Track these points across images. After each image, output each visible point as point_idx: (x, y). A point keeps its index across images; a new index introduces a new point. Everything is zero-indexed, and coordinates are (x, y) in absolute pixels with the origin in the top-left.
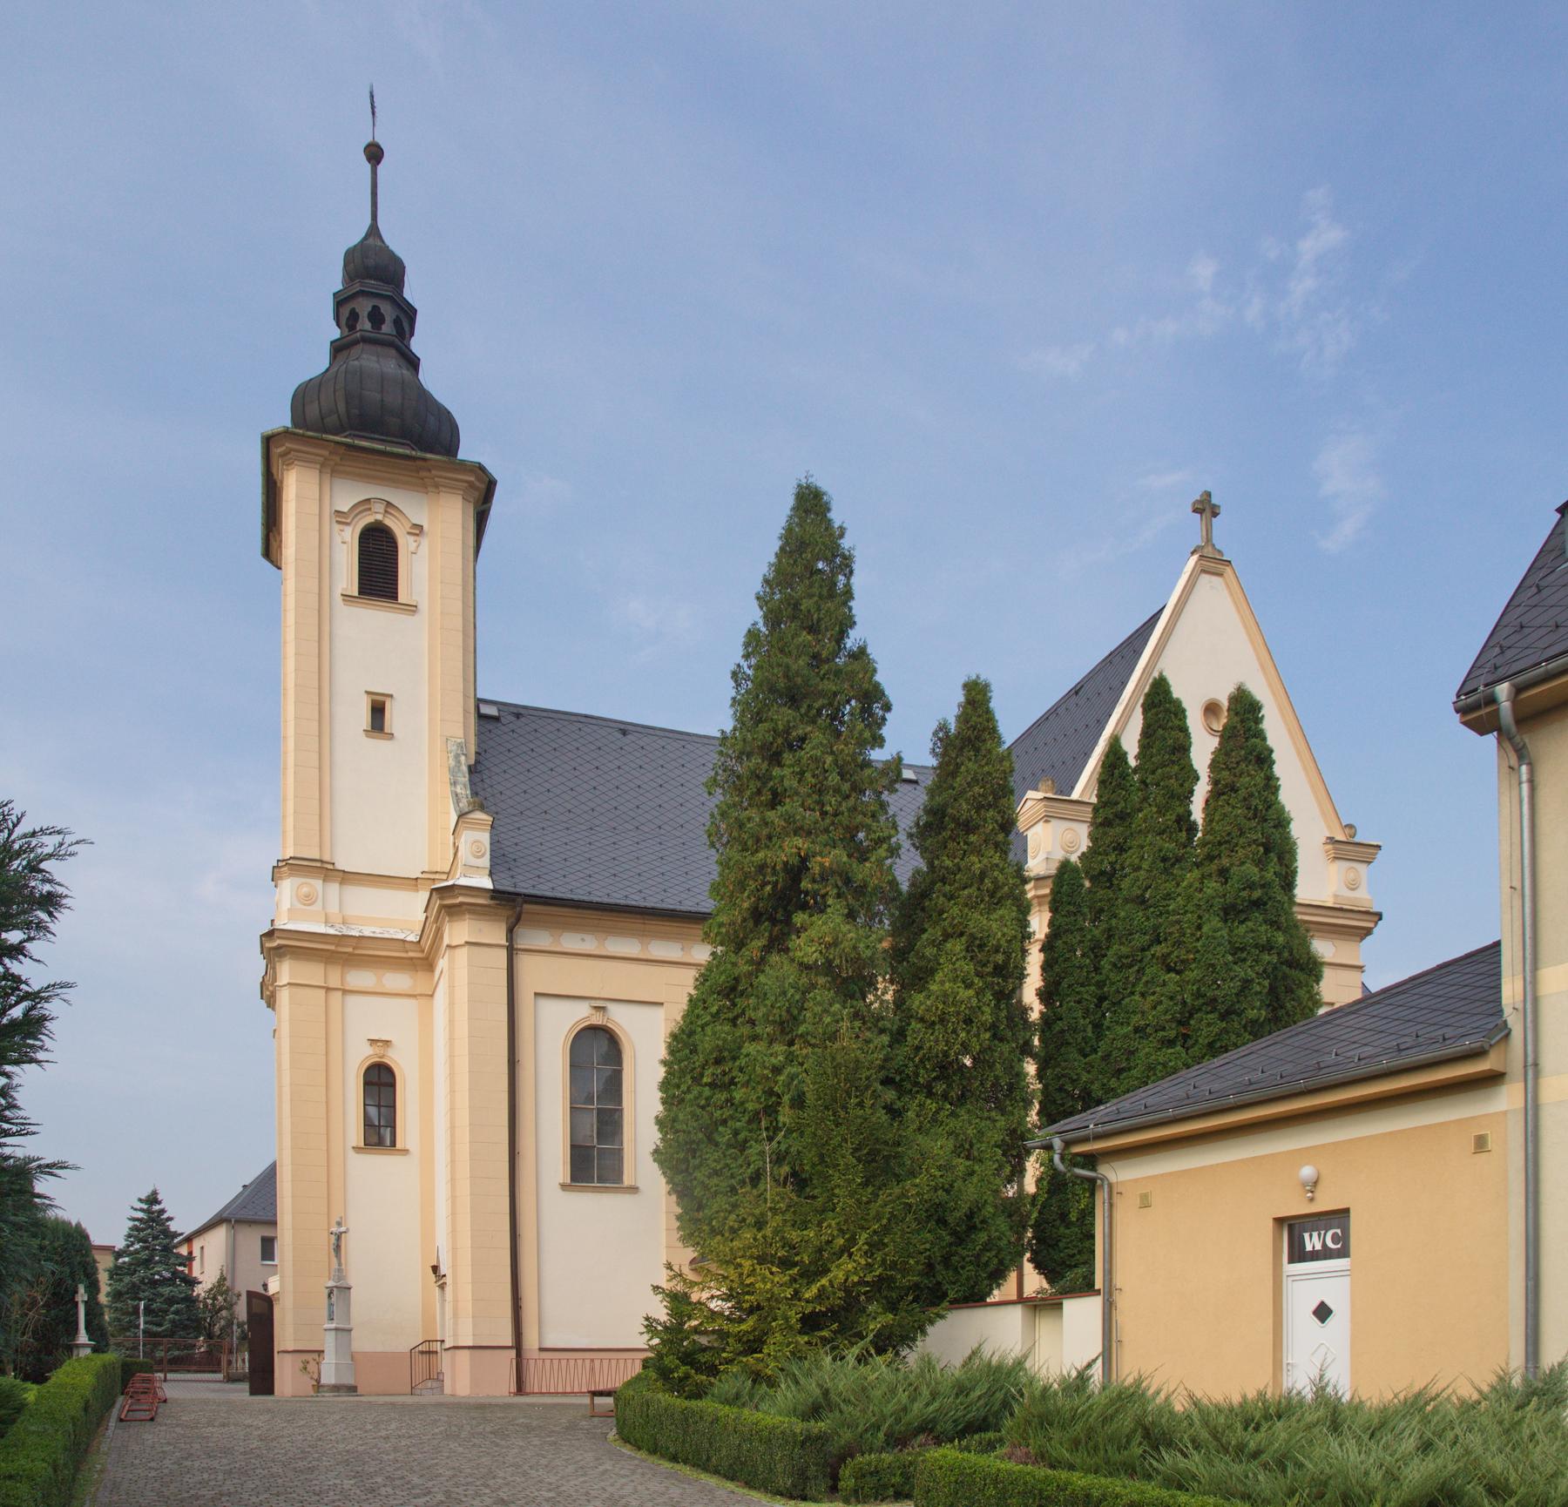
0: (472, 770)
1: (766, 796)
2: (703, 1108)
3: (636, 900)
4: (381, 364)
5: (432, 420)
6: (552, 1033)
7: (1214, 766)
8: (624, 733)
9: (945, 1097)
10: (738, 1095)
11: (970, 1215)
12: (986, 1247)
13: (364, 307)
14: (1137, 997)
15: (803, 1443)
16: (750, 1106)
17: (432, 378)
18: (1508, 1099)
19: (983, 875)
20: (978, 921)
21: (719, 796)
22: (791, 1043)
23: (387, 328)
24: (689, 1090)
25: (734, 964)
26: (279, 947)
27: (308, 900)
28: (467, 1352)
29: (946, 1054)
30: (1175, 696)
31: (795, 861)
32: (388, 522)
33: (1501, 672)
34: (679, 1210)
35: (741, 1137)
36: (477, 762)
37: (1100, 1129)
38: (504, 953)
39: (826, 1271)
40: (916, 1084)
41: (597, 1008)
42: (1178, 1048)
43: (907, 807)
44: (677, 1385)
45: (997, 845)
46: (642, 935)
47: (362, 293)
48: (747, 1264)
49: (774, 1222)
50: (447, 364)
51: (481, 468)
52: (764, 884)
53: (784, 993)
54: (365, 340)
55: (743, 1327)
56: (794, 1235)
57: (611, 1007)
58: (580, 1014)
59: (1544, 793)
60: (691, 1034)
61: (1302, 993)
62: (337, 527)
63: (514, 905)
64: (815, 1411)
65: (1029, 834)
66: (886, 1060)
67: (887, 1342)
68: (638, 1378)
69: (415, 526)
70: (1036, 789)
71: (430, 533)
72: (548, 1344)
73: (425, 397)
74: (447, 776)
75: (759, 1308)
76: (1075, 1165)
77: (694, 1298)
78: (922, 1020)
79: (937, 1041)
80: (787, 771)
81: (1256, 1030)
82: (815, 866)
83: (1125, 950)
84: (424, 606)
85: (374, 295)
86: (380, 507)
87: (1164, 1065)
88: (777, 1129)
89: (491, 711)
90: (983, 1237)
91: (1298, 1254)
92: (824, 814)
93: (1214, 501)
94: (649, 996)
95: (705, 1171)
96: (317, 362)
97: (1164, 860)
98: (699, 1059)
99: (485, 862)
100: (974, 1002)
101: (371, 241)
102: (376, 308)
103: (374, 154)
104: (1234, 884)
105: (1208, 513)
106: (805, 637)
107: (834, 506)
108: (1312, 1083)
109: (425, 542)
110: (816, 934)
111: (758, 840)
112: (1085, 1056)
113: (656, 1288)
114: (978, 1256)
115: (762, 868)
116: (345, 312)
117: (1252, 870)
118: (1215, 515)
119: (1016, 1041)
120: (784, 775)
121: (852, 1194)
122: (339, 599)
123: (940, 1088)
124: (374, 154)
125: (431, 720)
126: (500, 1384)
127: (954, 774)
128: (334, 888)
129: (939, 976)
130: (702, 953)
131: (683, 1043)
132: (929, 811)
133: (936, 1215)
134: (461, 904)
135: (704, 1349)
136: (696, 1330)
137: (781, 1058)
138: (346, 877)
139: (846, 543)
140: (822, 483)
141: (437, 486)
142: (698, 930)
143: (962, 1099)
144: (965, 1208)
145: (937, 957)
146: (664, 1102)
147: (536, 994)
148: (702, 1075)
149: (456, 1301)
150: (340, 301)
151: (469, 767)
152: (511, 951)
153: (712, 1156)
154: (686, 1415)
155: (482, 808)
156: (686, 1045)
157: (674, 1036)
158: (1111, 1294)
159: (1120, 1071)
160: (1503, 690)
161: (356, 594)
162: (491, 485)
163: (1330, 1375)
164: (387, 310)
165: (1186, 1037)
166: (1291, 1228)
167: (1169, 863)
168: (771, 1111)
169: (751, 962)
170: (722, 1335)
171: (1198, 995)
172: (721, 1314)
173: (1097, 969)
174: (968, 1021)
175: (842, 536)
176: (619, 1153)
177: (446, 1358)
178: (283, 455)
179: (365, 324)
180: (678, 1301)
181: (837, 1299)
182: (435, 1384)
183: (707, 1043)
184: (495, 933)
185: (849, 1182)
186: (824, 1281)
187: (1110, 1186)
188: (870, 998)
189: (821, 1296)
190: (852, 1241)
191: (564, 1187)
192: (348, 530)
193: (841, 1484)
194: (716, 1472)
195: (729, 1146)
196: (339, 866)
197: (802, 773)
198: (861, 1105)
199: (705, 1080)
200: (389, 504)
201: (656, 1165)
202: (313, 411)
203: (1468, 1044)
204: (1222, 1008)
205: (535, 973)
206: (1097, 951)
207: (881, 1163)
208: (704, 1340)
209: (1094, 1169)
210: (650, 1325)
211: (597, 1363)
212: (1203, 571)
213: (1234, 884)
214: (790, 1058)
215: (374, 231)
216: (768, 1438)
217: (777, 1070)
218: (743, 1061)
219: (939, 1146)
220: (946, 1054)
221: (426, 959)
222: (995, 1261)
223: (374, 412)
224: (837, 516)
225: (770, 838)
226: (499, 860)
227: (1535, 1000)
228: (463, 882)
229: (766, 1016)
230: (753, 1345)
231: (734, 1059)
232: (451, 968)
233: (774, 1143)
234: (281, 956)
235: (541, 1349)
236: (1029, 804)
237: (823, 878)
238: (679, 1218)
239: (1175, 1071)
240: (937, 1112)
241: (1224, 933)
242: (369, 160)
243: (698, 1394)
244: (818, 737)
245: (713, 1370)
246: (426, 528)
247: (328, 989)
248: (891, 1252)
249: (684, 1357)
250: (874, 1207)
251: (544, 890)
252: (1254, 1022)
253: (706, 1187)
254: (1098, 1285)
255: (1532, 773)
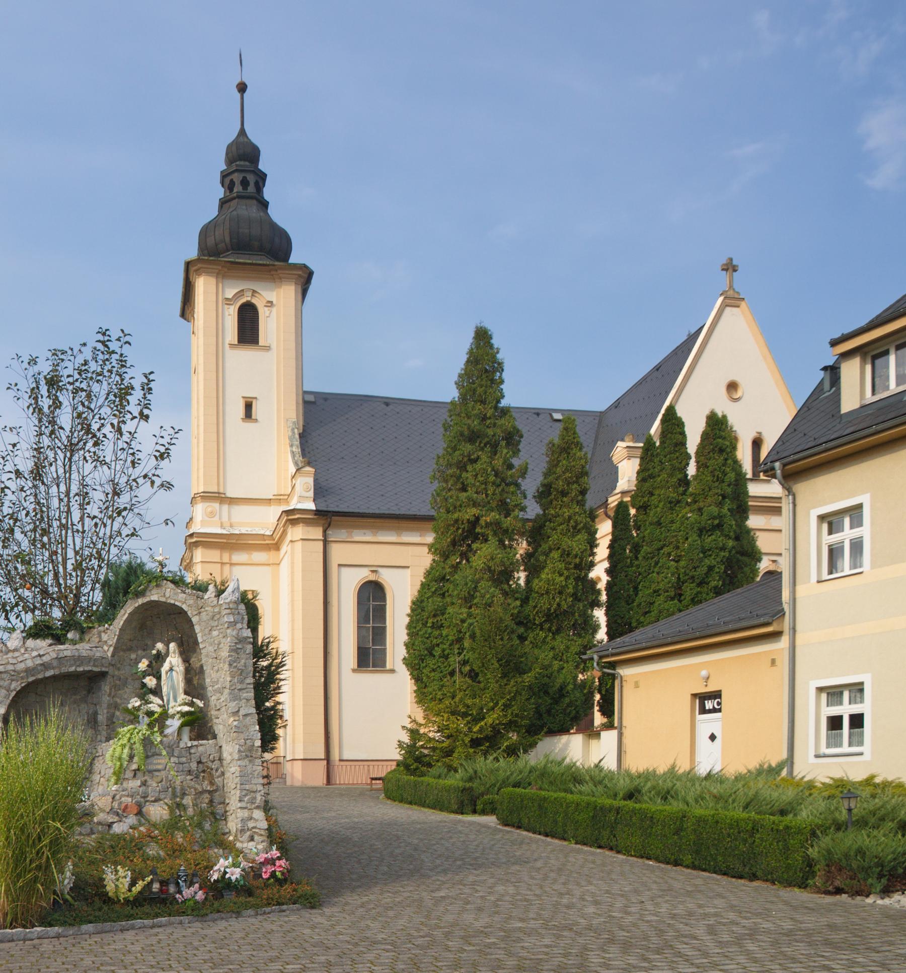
0: (301, 436)
1: (459, 486)
2: (427, 638)
3: (395, 511)
4: (249, 210)
5: (277, 240)
6: (348, 584)
7: (697, 453)
8: (387, 404)
9: (550, 630)
10: (444, 633)
11: (561, 688)
12: (568, 705)
13: (237, 178)
14: (655, 574)
15: (462, 791)
16: (450, 638)
17: (277, 214)
18: (784, 643)
19: (570, 518)
20: (567, 542)
21: (436, 485)
22: (470, 607)
23: (251, 189)
24: (420, 630)
25: (444, 568)
26: (196, 542)
27: (212, 514)
28: (300, 762)
29: (549, 609)
30: (679, 415)
31: (472, 519)
32: (254, 301)
33: (776, 457)
34: (415, 688)
35: (446, 652)
36: (304, 430)
37: (614, 651)
38: (321, 543)
39: (484, 718)
40: (535, 624)
41: (373, 571)
42: (676, 601)
43: (531, 484)
44: (413, 772)
45: (578, 502)
46: (399, 530)
47: (236, 171)
48: (446, 715)
49: (459, 696)
50: (284, 204)
51: (305, 266)
52: (458, 528)
53: (466, 584)
54: (239, 197)
55: (444, 745)
56: (469, 702)
57: (380, 570)
58: (364, 575)
59: (798, 508)
60: (422, 601)
61: (747, 569)
62: (226, 306)
63: (328, 517)
64: (470, 779)
65: (620, 465)
66: (519, 612)
67: (512, 751)
68: (395, 770)
69: (269, 302)
70: (623, 440)
71: (276, 303)
72: (345, 758)
73: (274, 226)
74: (288, 441)
75: (452, 736)
76: (604, 667)
77: (422, 731)
78: (537, 592)
79: (544, 603)
80: (469, 475)
81: (718, 592)
82: (482, 522)
83: (649, 550)
84: (274, 346)
85: (244, 169)
86: (250, 294)
87: (668, 610)
88: (463, 649)
89: (311, 398)
90: (567, 700)
91: (703, 711)
92: (487, 495)
93: (735, 263)
94: (404, 566)
95: (428, 669)
96: (211, 212)
97: (670, 502)
98: (426, 614)
99: (311, 494)
100: (564, 583)
101: (241, 139)
102: (245, 178)
103: (242, 88)
104: (705, 517)
105: (730, 270)
106: (479, 406)
107: (494, 337)
108: (703, 634)
109: (274, 310)
110: (484, 553)
111: (455, 508)
112: (629, 604)
113: (403, 727)
114: (565, 710)
115: (457, 521)
116: (227, 181)
117: (714, 510)
118: (735, 271)
119: (587, 600)
120: (468, 476)
121: (497, 682)
122: (227, 346)
123: (547, 626)
124: (242, 88)
125: (278, 410)
126: (319, 779)
127: (556, 466)
128: (225, 507)
129: (546, 570)
130: (430, 538)
131: (418, 606)
132: (543, 485)
133: (544, 689)
134: (298, 519)
135: (426, 756)
136: (422, 747)
137: (465, 615)
138: (233, 501)
139: (499, 356)
140: (488, 325)
141: (280, 278)
142: (430, 525)
143: (558, 631)
144: (558, 686)
145: (545, 561)
146: (408, 634)
147: (340, 565)
148: (427, 622)
149: (294, 734)
150: (224, 176)
151: (300, 434)
152: (326, 542)
153: (431, 662)
154: (416, 784)
155: (309, 464)
156: (419, 606)
157: (413, 603)
158: (621, 729)
159: (646, 613)
160: (777, 465)
161: (236, 343)
162: (310, 274)
163: (678, 763)
164: (251, 178)
165: (680, 595)
166: (700, 698)
167: (673, 504)
168: (459, 640)
169: (452, 566)
170: (434, 749)
171: (685, 574)
172: (434, 739)
173: (637, 558)
174: (560, 593)
175: (498, 352)
176: (384, 651)
177: (288, 766)
178: (196, 271)
179: (238, 188)
180: (414, 733)
181: (489, 732)
182: (281, 780)
183: (430, 606)
184: (317, 533)
185: (495, 676)
186: (483, 723)
187: (621, 677)
188: (511, 583)
189: (481, 730)
190: (497, 704)
191: (354, 671)
192: (232, 307)
193: (478, 807)
194: (429, 807)
195: (440, 657)
196: (229, 495)
197: (476, 475)
198: (502, 639)
199: (428, 625)
200: (254, 291)
201: (404, 666)
202: (211, 241)
203: (762, 620)
204: (698, 581)
205: (339, 553)
206: (636, 548)
207: (512, 666)
208: (426, 752)
209: (614, 669)
210: (400, 744)
211: (371, 767)
212: (727, 306)
213: (705, 517)
214: (470, 615)
215: (242, 132)
216: (448, 789)
217: (463, 621)
218: (447, 616)
219: (544, 656)
220: (549, 609)
221: (276, 544)
222: (574, 712)
223: (246, 240)
224: (495, 342)
225: (461, 506)
226: (319, 492)
227: (794, 600)
228: (299, 506)
229: (458, 595)
230: (449, 753)
231: (443, 614)
232: (292, 553)
233: (462, 656)
234: (197, 547)
235: (341, 760)
236: (619, 449)
237: (488, 525)
238: (415, 692)
239: (673, 614)
240: (546, 637)
241: (699, 542)
242: (239, 91)
243: (423, 775)
244: (484, 458)
245: (430, 765)
246: (274, 302)
247: (222, 564)
248: (515, 709)
249: (415, 759)
250: (508, 687)
251: (343, 508)
252: (716, 587)
253: (428, 677)
254: (616, 725)
255: (794, 499)
